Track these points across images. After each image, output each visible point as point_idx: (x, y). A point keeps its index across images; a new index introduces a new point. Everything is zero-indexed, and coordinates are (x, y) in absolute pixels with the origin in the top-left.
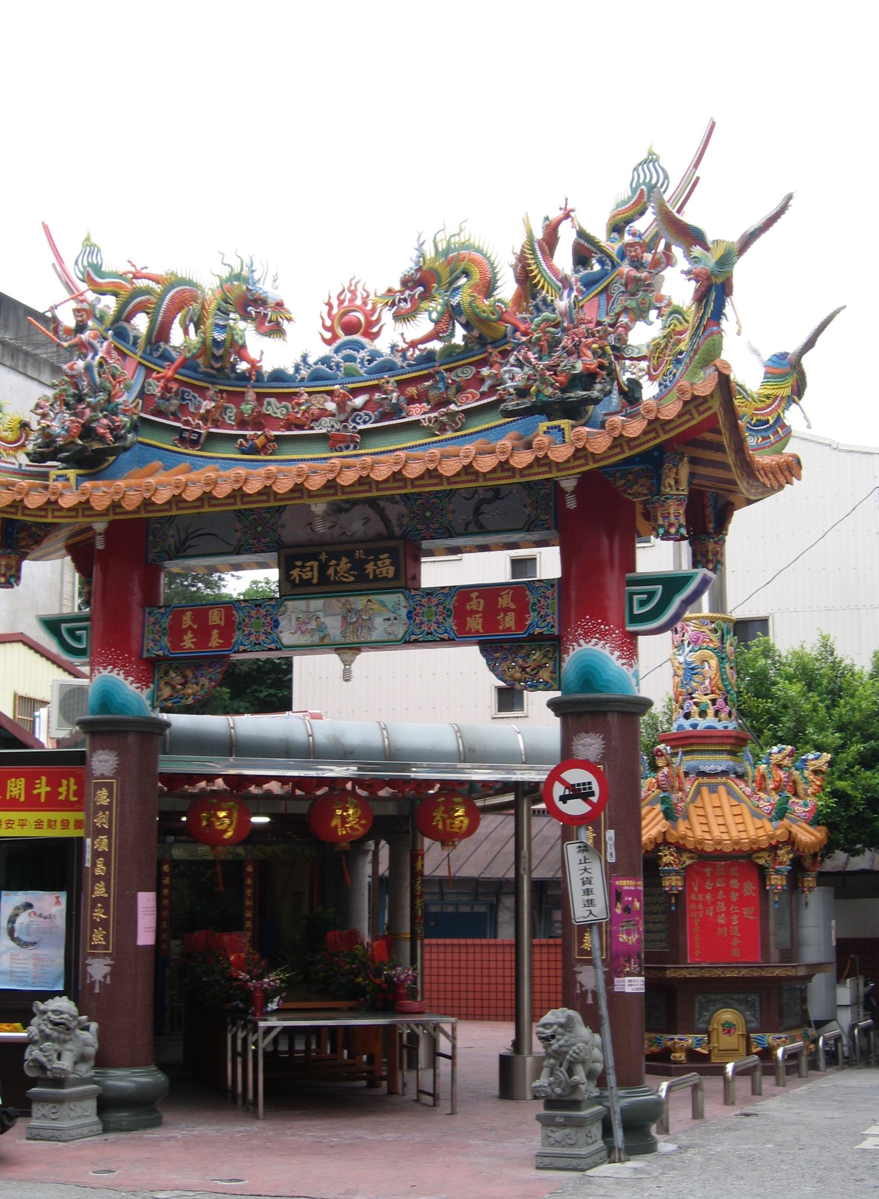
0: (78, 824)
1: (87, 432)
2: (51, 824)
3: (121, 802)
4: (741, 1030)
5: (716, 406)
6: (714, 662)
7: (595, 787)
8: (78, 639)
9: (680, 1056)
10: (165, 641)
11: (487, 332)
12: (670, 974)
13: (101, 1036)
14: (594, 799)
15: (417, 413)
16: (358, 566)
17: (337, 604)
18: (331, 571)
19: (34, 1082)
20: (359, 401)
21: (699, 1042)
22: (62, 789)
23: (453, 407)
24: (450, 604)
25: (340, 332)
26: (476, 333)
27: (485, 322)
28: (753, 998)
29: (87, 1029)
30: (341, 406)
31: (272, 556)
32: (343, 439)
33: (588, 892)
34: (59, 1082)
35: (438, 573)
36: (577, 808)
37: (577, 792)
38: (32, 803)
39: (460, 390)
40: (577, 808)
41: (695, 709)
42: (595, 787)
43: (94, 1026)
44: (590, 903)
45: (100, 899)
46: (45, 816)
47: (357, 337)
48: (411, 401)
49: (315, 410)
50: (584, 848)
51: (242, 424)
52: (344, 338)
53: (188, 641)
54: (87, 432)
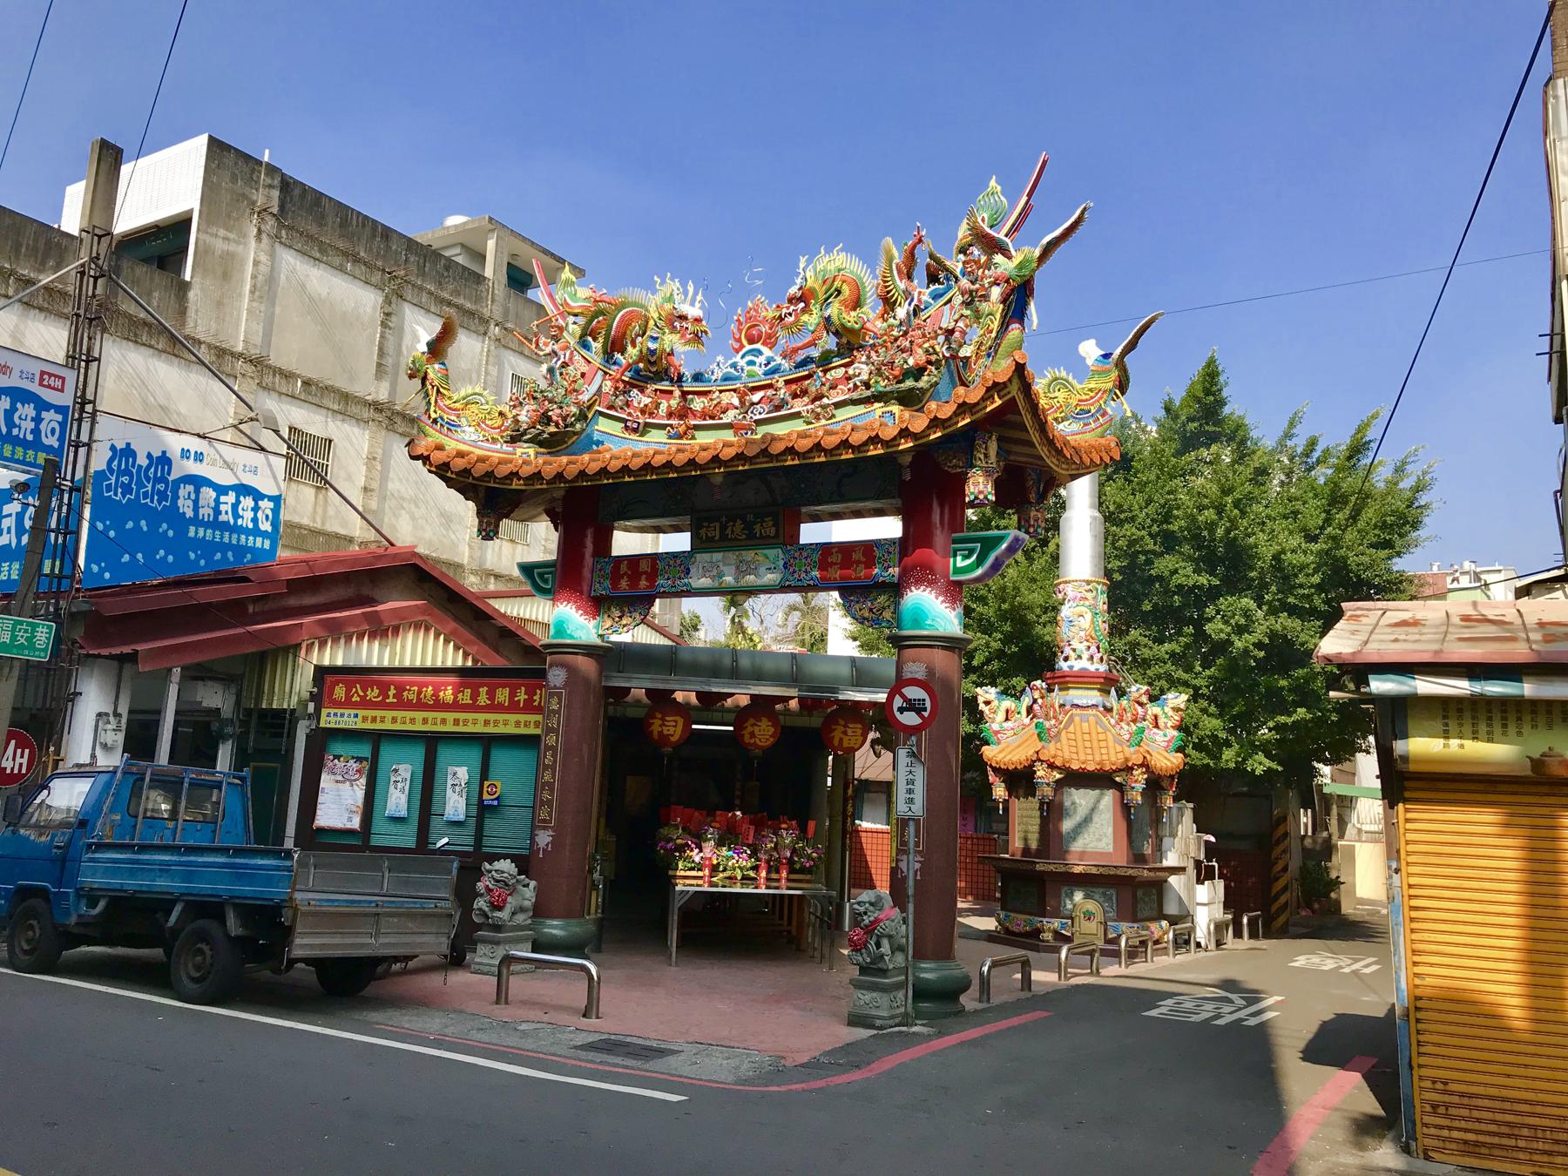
0: (537, 724)
1: (546, 419)
2: (527, 724)
3: (568, 707)
4: (1100, 917)
5: (1014, 390)
6: (1089, 616)
7: (928, 704)
8: (546, 581)
9: (1048, 936)
10: (607, 583)
11: (853, 340)
12: (1038, 868)
13: (539, 892)
14: (926, 714)
15: (799, 406)
16: (748, 526)
17: (732, 556)
18: (729, 531)
19: (479, 927)
20: (756, 397)
21: (1063, 926)
22: (537, 698)
23: (825, 401)
24: (816, 557)
25: (745, 342)
26: (844, 340)
27: (851, 331)
28: (1112, 892)
29: (527, 886)
30: (742, 403)
31: (687, 520)
32: (743, 427)
33: (910, 791)
34: (497, 928)
35: (810, 533)
36: (910, 719)
37: (912, 706)
38: (513, 707)
39: (833, 387)
40: (910, 719)
41: (1072, 654)
42: (928, 704)
43: (533, 884)
44: (911, 801)
45: (548, 783)
46: (522, 718)
47: (758, 346)
48: (795, 396)
49: (725, 402)
50: (912, 755)
51: (670, 415)
52: (748, 347)
53: (624, 583)
54: (546, 419)
